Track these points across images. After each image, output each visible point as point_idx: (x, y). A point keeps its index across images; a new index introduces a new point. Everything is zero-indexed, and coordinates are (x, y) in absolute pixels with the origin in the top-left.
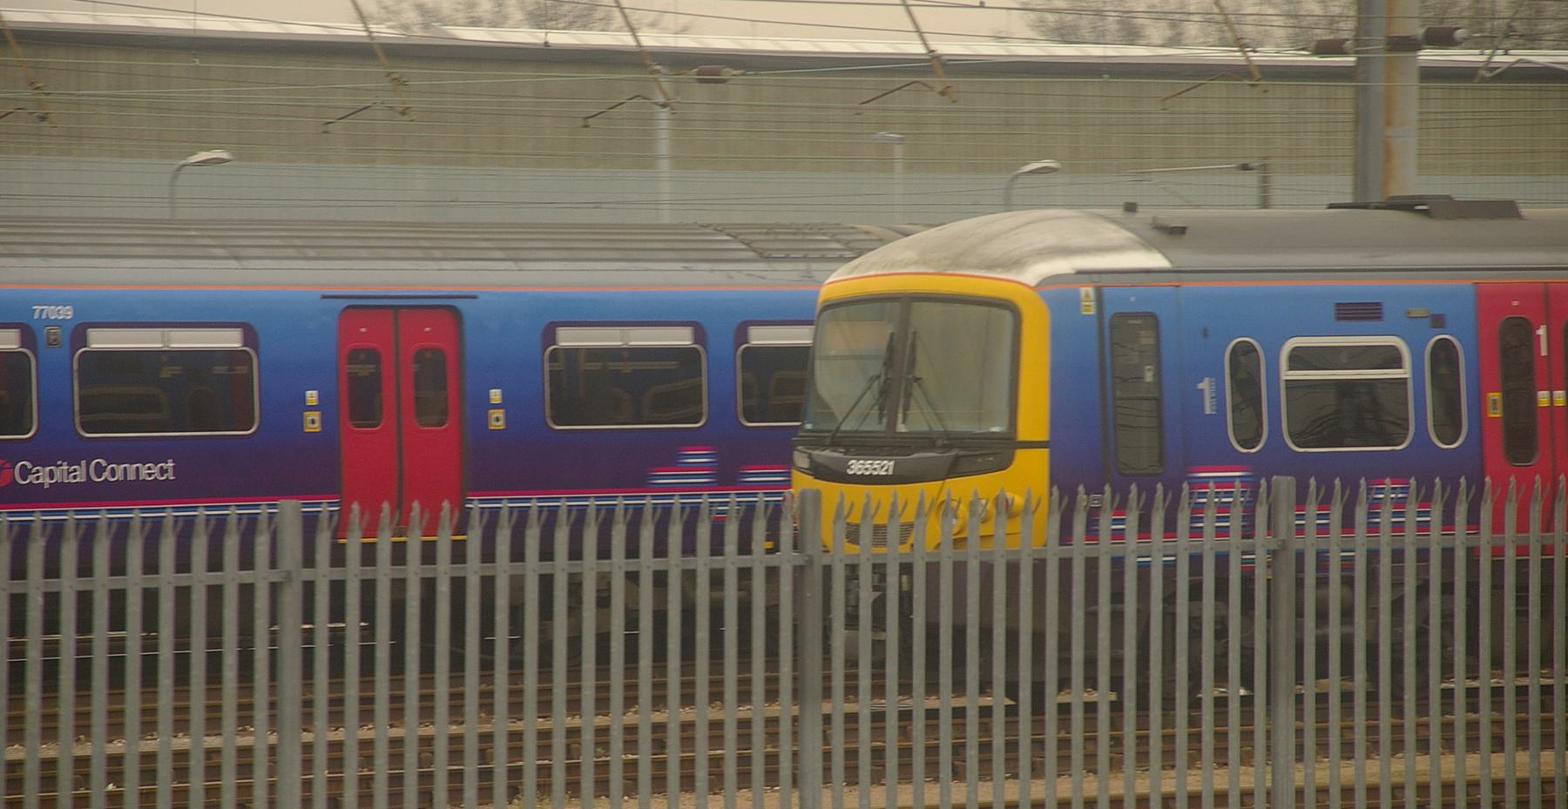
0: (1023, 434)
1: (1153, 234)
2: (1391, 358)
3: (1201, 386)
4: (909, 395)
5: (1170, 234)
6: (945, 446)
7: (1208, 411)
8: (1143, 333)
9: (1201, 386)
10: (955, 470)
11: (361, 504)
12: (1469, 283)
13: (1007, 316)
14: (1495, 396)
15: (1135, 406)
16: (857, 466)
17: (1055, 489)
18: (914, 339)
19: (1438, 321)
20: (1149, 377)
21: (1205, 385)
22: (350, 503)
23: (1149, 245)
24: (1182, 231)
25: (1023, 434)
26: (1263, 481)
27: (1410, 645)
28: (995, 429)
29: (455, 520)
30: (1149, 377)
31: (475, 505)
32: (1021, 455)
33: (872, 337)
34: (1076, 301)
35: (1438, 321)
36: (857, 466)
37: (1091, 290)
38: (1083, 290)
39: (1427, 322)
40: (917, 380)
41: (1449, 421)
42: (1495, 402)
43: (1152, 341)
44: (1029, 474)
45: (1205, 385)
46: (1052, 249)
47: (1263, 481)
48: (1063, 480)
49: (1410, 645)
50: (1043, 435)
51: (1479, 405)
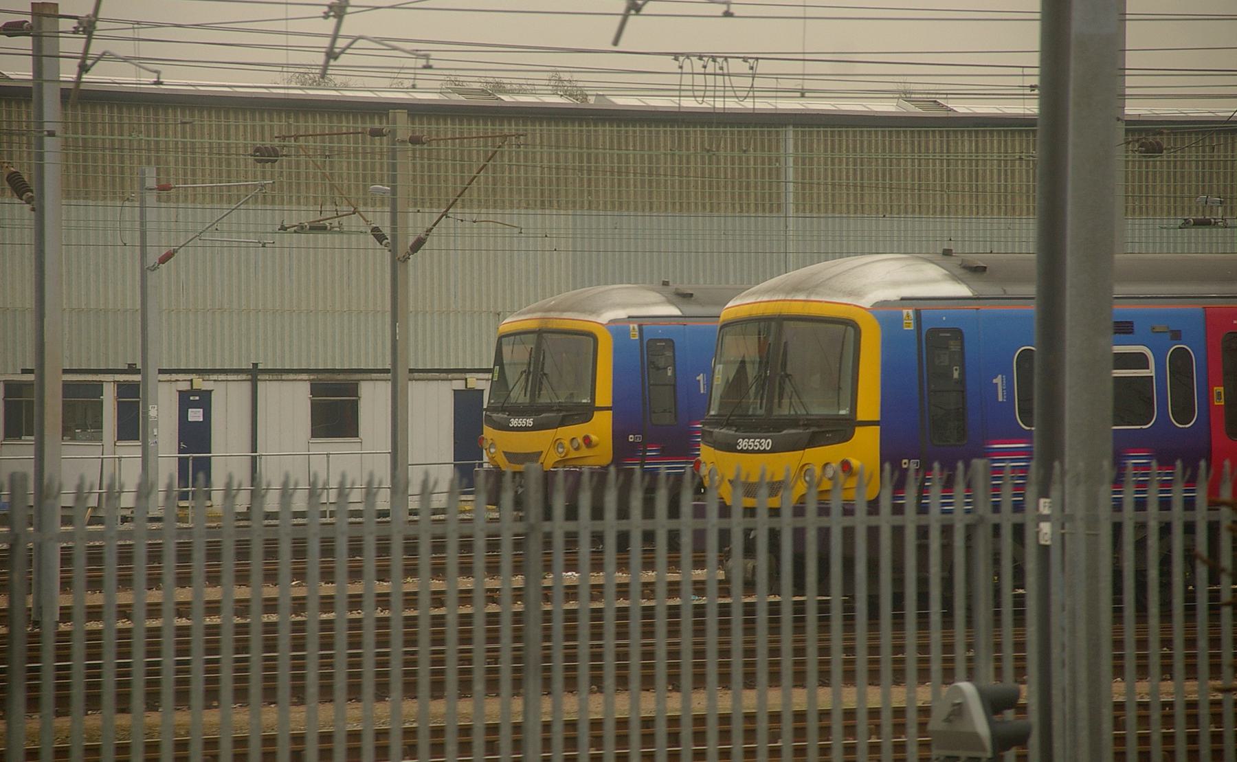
0: (861, 416)
1: (960, 272)
2: (1139, 361)
3: (995, 381)
4: (782, 389)
5: (974, 271)
6: (804, 425)
7: (1000, 399)
8: (952, 343)
9: (995, 381)
10: (563, 423)
11: (1183, 461)
12: (1200, 308)
13: (851, 330)
14: (1221, 389)
15: (946, 401)
16: (514, 422)
17: (887, 466)
18: (785, 354)
19: (1176, 335)
20: (956, 375)
21: (998, 380)
22: (1198, 461)
23: (956, 278)
24: (984, 269)
25: (861, 416)
26: (960, 465)
27: (1153, 574)
28: (842, 412)
29: (646, 483)
30: (956, 375)
31: (663, 469)
32: (858, 430)
33: (745, 348)
34: (899, 320)
35: (1176, 335)
36: (514, 422)
37: (911, 312)
38: (905, 312)
39: (1168, 336)
40: (787, 376)
41: (1184, 412)
42: (1219, 393)
43: (958, 348)
44: (864, 448)
45: (998, 380)
46: (885, 279)
47: (960, 465)
48: (890, 454)
49: (1153, 574)
50: (876, 416)
51: (1207, 396)
